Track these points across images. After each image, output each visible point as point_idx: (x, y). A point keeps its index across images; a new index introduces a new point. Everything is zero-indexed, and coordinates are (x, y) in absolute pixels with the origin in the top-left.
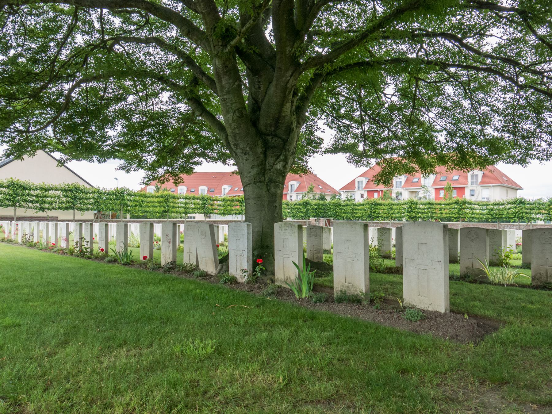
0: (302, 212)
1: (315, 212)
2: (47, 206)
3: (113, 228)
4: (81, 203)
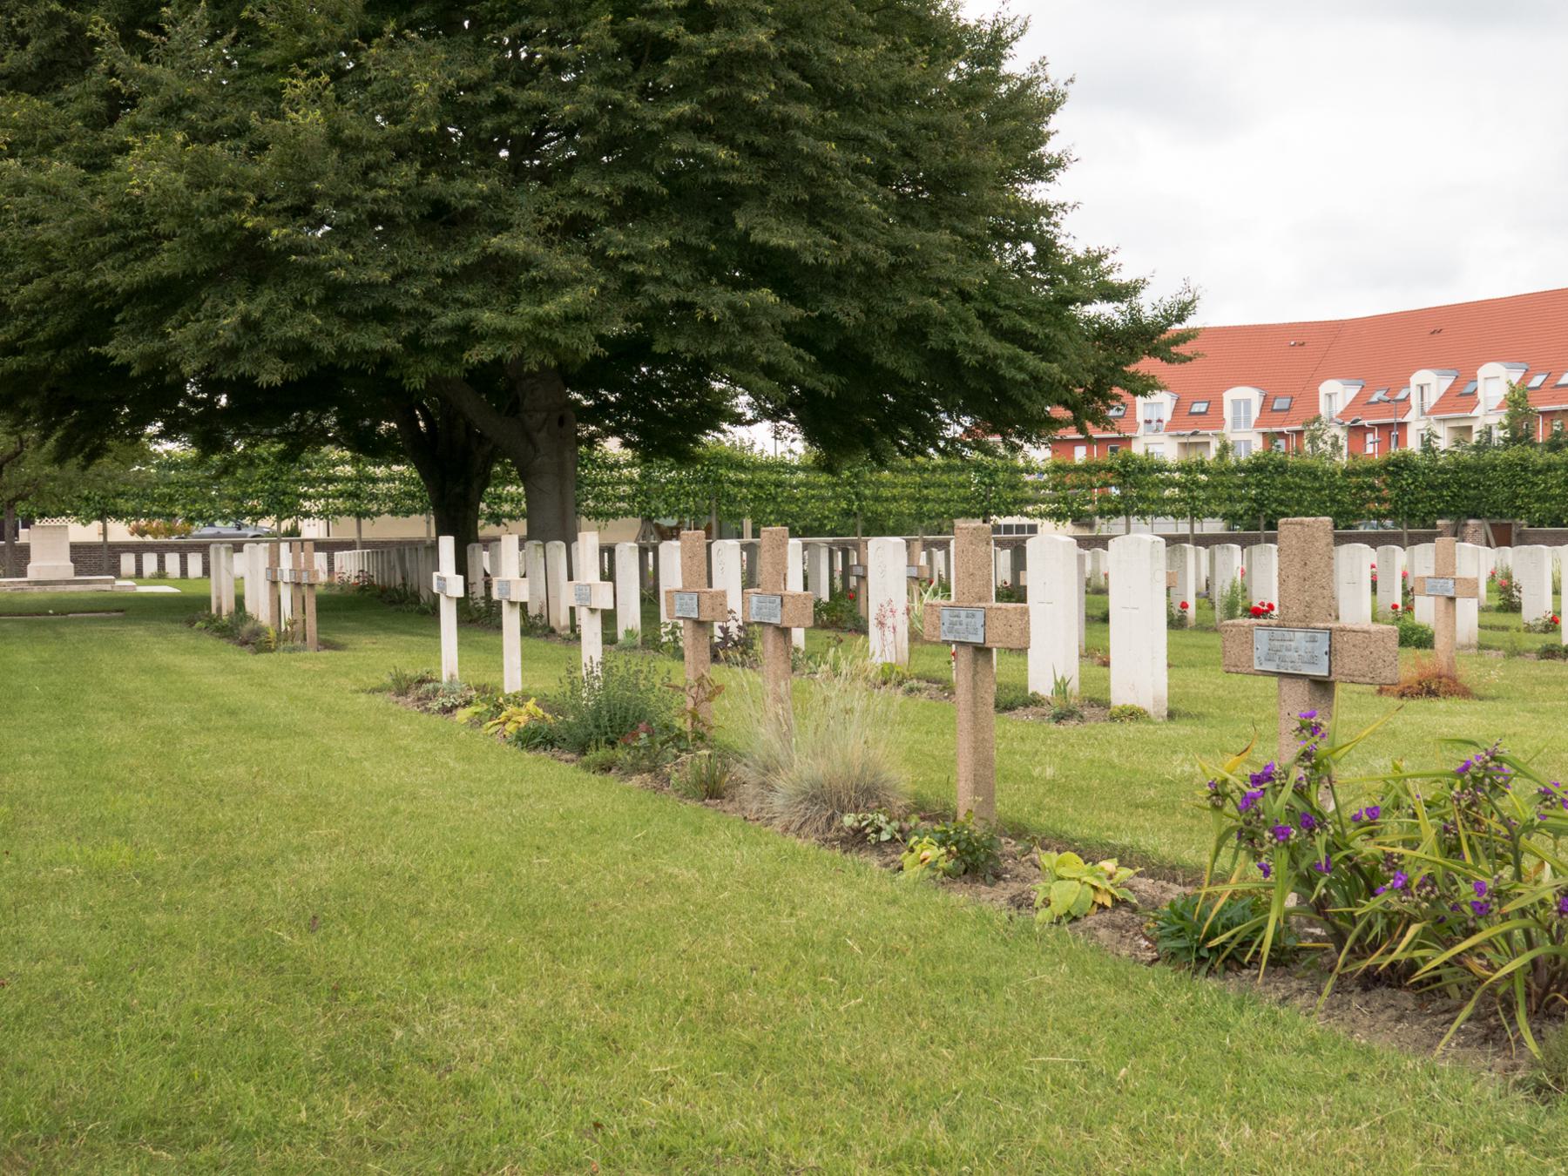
0: (1381, 500)
1: (1441, 496)
2: (507, 507)
3: (728, 554)
4: (596, 498)
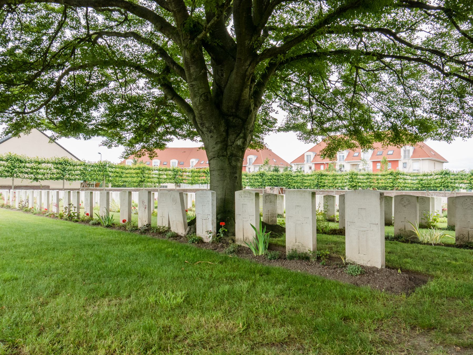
0: (258, 182)
1: (270, 182)
2: (40, 176)
3: (97, 195)
4: (69, 174)
